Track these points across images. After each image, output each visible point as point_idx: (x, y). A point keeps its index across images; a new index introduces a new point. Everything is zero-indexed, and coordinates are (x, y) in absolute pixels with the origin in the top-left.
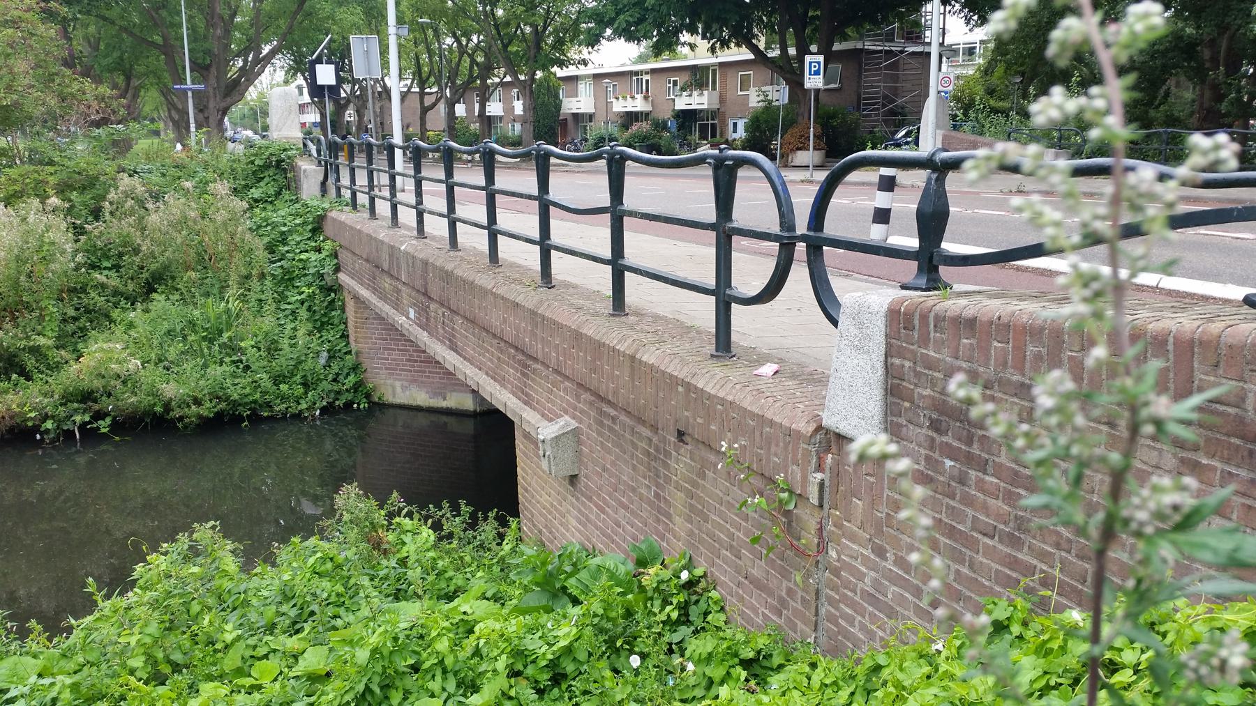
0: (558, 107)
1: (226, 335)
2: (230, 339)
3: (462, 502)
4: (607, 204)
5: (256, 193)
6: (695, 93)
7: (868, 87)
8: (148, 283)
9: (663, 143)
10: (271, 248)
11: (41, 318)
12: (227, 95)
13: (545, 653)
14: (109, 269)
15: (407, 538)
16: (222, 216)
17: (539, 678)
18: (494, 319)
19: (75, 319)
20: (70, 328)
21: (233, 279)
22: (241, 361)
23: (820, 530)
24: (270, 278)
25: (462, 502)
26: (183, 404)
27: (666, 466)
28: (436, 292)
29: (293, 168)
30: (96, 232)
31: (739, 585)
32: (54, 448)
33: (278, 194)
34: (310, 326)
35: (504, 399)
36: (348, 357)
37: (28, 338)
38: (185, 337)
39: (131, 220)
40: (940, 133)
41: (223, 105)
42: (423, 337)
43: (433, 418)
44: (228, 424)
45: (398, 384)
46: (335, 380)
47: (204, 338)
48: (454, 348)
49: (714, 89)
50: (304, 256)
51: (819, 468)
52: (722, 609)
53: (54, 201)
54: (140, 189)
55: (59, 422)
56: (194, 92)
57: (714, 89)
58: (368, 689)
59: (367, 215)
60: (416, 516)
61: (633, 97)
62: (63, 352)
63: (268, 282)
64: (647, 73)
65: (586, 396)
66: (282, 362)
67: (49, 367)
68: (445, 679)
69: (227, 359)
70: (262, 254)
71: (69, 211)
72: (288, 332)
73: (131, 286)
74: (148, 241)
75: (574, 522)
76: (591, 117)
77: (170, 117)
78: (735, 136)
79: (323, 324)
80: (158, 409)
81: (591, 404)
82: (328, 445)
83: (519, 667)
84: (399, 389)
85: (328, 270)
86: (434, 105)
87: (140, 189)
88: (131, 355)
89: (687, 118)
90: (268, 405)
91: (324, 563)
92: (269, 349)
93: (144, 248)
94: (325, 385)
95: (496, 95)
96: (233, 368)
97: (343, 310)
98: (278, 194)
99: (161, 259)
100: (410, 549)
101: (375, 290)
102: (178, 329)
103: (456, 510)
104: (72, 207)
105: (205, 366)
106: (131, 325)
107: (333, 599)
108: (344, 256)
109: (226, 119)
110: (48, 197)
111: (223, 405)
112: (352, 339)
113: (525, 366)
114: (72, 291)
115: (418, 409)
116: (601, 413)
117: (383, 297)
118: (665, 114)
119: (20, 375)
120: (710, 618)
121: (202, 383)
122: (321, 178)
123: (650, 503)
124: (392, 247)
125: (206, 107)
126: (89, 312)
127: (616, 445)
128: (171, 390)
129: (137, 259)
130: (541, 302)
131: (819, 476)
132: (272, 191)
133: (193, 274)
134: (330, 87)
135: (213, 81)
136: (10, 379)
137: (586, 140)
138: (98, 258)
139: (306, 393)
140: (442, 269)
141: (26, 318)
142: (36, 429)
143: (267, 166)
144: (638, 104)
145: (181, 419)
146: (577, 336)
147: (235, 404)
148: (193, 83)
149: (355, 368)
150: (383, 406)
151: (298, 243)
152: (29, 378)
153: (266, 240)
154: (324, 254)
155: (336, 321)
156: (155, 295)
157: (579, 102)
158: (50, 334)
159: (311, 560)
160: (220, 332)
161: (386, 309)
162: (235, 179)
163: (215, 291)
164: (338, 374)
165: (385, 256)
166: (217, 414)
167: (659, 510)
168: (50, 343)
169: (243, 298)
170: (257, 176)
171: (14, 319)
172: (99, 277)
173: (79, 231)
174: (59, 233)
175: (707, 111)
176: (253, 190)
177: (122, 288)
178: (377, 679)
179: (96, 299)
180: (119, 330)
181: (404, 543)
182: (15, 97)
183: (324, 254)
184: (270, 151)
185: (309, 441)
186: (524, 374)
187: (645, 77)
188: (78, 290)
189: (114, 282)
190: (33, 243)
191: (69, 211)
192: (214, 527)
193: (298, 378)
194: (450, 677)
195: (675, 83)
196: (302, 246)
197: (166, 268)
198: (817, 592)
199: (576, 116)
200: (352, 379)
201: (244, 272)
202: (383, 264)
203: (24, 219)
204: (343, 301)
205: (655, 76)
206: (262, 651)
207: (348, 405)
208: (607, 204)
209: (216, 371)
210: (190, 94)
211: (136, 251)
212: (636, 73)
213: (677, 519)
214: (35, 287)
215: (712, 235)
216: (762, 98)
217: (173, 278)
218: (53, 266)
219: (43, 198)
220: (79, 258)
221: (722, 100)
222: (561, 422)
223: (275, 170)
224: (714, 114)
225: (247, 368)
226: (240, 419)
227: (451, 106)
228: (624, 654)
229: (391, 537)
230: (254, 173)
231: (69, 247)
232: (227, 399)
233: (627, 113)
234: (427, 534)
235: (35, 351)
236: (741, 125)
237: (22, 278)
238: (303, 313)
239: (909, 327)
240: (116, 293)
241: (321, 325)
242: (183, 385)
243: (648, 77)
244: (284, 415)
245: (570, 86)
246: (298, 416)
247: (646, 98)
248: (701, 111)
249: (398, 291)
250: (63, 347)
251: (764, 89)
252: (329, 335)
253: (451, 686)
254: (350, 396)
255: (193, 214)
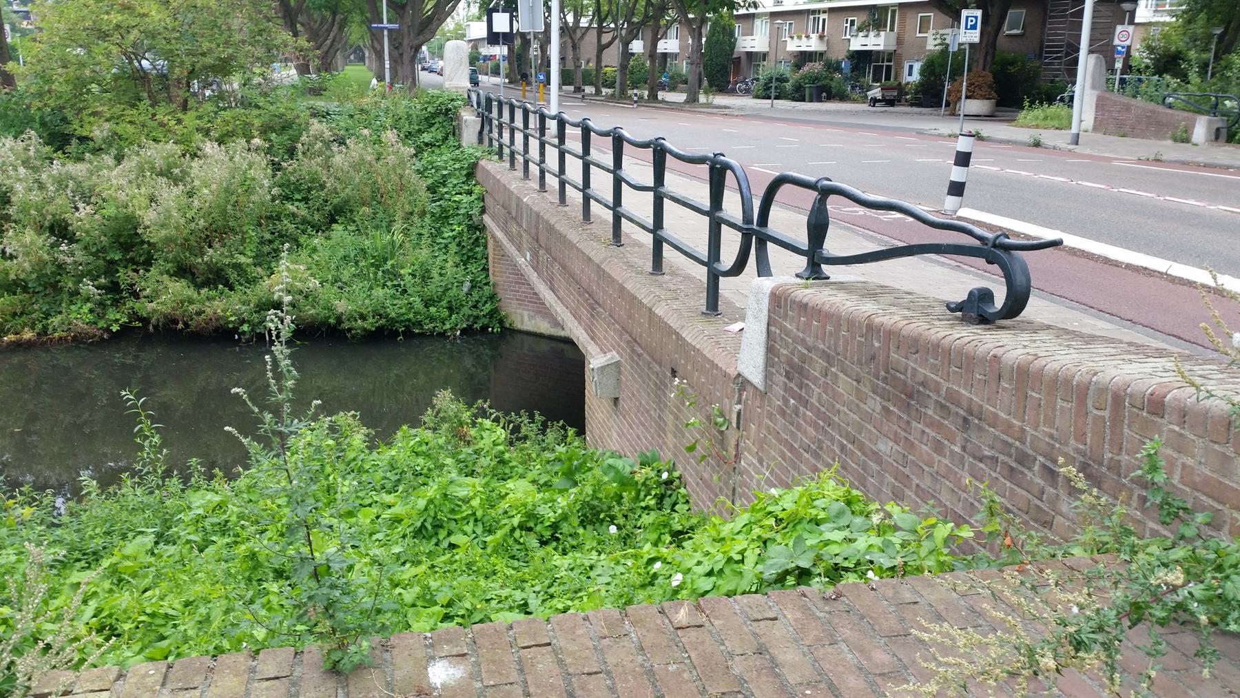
0: (732, 45)
1: (390, 263)
2: (393, 266)
3: (537, 413)
4: (652, 185)
5: (426, 137)
6: (872, 34)
7: (1050, 29)
8: (331, 214)
9: (833, 84)
10: (432, 189)
11: (243, 240)
12: (421, 32)
13: (551, 517)
14: (300, 201)
15: (485, 434)
16: (392, 159)
17: (544, 533)
18: (576, 266)
19: (270, 242)
20: (266, 249)
21: (399, 216)
22: (399, 285)
23: (737, 445)
24: (428, 216)
25: (537, 413)
26: (351, 318)
27: (665, 395)
28: (544, 242)
29: (457, 117)
30: (290, 169)
31: (697, 484)
32: (248, 346)
33: (445, 138)
34: (457, 259)
35: (579, 334)
36: (486, 288)
37: (232, 256)
38: (357, 263)
39: (319, 160)
40: (1096, 93)
41: (416, 42)
42: (533, 276)
43: (553, 344)
44: (387, 336)
45: (526, 313)
46: (475, 307)
47: (372, 265)
48: (552, 289)
49: (892, 29)
50: (457, 198)
51: (739, 402)
52: (687, 502)
53: (257, 141)
54: (327, 134)
55: (253, 326)
56: (390, 31)
57: (892, 29)
58: (423, 526)
59: (508, 165)
60: (502, 421)
61: (808, 37)
62: (259, 269)
63: (427, 219)
64: (824, 12)
65: (626, 337)
66: (433, 288)
67: (248, 281)
68: (475, 525)
69: (389, 283)
70: (424, 195)
71: (269, 151)
72: (438, 261)
73: (316, 217)
74: (332, 179)
75: (615, 434)
76: (764, 56)
77: (373, 47)
78: (910, 79)
79: (469, 257)
80: (332, 321)
81: (628, 342)
82: (468, 362)
83: (531, 524)
84: (526, 318)
85: (475, 211)
86: (610, 43)
87: (327, 134)
88: (312, 275)
89: (862, 59)
90: (420, 324)
91: (421, 445)
92: (423, 277)
93: (328, 185)
94: (466, 310)
95: (672, 32)
96: (393, 291)
97: (486, 247)
98: (445, 138)
99: (342, 195)
100: (485, 443)
101: (507, 233)
102: (352, 255)
103: (532, 417)
104: (272, 146)
105: (371, 288)
106: (315, 250)
107: (425, 471)
108: (488, 200)
109: (424, 48)
110: (253, 137)
111: (383, 321)
112: (491, 272)
113: (593, 309)
114: (269, 218)
115: (541, 336)
116: (633, 351)
117: (511, 240)
118: (839, 55)
119: (225, 286)
120: (677, 508)
121: (367, 301)
122: (478, 128)
123: (656, 422)
124: (518, 198)
125: (400, 44)
126: (281, 236)
127: (640, 376)
128: (342, 306)
129: (323, 194)
130: (605, 259)
131: (738, 407)
132: (439, 137)
133: (366, 210)
134: (504, 34)
135: (408, 20)
136: (217, 288)
137: (757, 80)
138: (291, 190)
139: (450, 316)
140: (547, 222)
141: (233, 239)
142: (235, 330)
143: (435, 115)
144: (812, 44)
145: (350, 330)
146: (622, 289)
147: (393, 321)
148: (389, 21)
149: (492, 297)
150: (513, 332)
151: (455, 185)
152: (232, 289)
153: (430, 181)
154: (474, 196)
155: (479, 256)
156: (334, 226)
157: (754, 40)
158: (249, 253)
159: (412, 443)
160: (386, 260)
161: (511, 249)
162: (410, 123)
163: (384, 224)
164: (477, 302)
165: (514, 205)
166: (377, 328)
167: (659, 426)
168: (250, 261)
169: (406, 232)
170: (429, 122)
171: (221, 240)
172: (291, 207)
173: (276, 167)
174: (260, 171)
175: (883, 52)
176: (425, 135)
177: (309, 218)
178: (430, 520)
179: (288, 226)
180: (304, 254)
181: (482, 438)
182: (230, 51)
183: (474, 196)
184: (441, 100)
185: (451, 357)
186: (592, 316)
187: (822, 16)
188: (275, 218)
189: (303, 212)
190: (238, 179)
191: (269, 151)
192: (354, 416)
193: (444, 303)
194: (480, 524)
195: (852, 23)
196: (457, 189)
197: (346, 202)
198: (734, 490)
199: (750, 54)
200: (488, 307)
201: (408, 208)
202: (513, 213)
203: (231, 159)
204: (486, 239)
205: (833, 15)
206: (367, 501)
207: (484, 328)
208: (652, 185)
209: (379, 292)
210: (386, 33)
211: (322, 187)
212: (814, 12)
213: (670, 435)
214: (239, 215)
215: (707, 219)
216: (939, 41)
217: (351, 211)
218: (253, 198)
219: (249, 139)
220: (275, 191)
221: (900, 41)
222: (609, 356)
223: (442, 116)
224: (890, 56)
225: (405, 291)
226: (397, 333)
227: (626, 44)
228: (605, 524)
229: (473, 432)
230: (426, 119)
231: (266, 183)
232: (387, 316)
233: (802, 53)
234: (501, 433)
235: (237, 267)
236: (917, 67)
237: (229, 207)
238: (453, 248)
239: (779, 302)
240: (304, 221)
241: (467, 259)
242: (351, 302)
243: (825, 16)
244: (432, 333)
245: (747, 24)
246: (442, 335)
247: (821, 37)
248: (878, 52)
249: (521, 236)
250: (260, 265)
251: (941, 32)
252: (472, 268)
253: (479, 530)
254: (486, 321)
255: (369, 158)
